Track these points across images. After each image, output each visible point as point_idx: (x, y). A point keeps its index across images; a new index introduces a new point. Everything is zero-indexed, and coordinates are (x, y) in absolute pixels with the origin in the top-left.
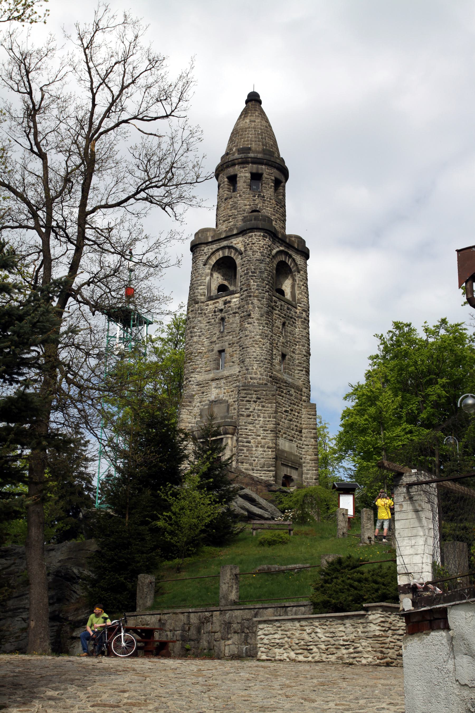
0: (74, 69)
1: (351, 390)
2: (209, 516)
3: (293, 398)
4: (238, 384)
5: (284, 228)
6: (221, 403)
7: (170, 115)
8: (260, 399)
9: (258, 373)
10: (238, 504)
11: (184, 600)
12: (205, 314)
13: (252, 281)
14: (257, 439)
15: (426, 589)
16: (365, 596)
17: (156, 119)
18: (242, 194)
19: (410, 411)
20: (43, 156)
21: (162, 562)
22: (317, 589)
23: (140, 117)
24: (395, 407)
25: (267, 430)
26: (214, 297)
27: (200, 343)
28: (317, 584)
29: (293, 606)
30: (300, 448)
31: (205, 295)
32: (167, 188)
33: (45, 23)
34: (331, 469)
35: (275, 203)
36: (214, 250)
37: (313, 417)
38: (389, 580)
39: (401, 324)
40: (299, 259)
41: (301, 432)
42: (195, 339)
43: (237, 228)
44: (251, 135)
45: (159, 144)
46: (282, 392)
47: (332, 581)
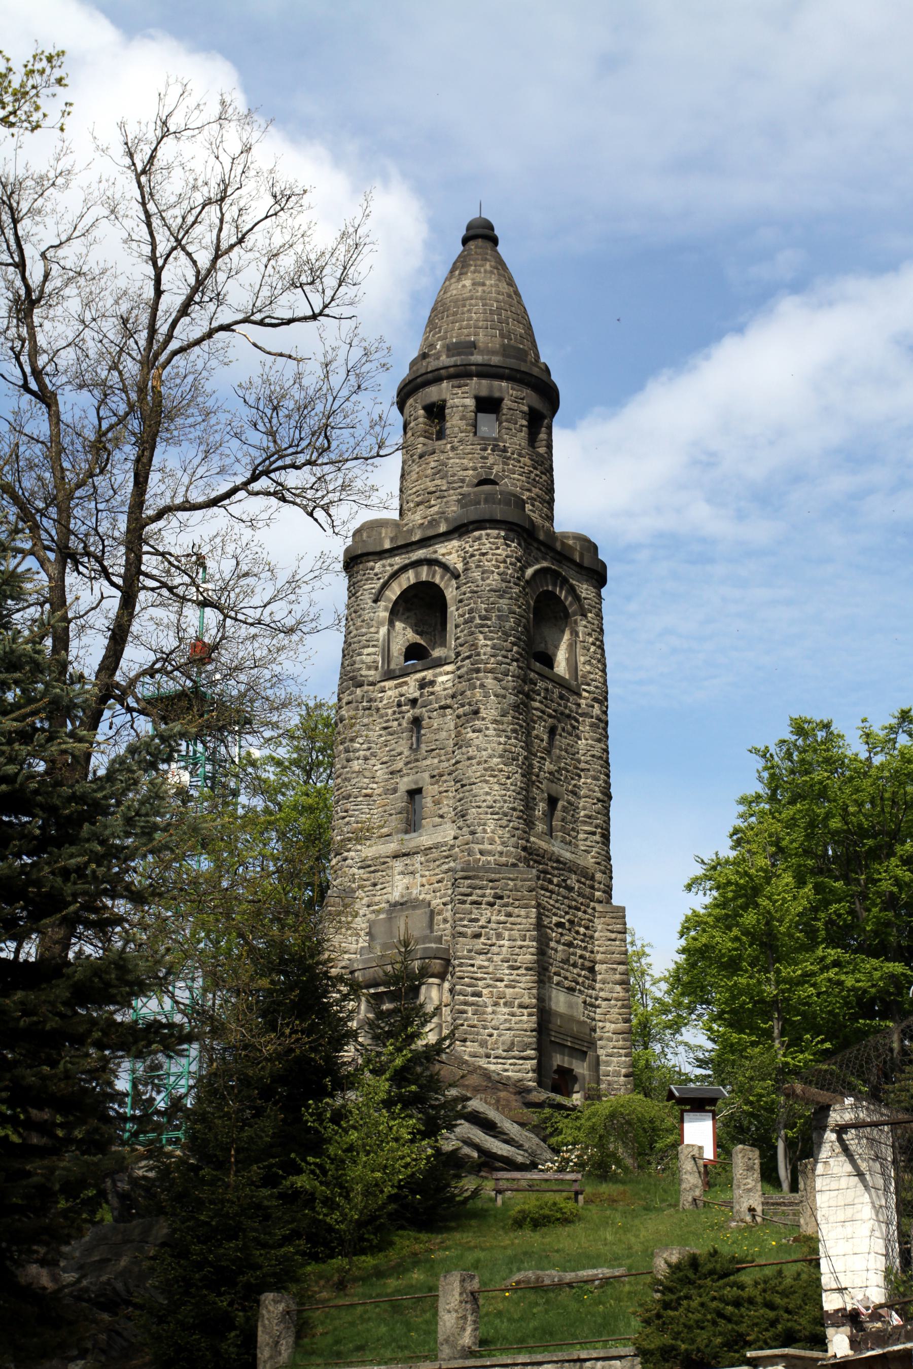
0: (112, 212)
1: (699, 870)
2: (406, 1166)
3: (574, 895)
4: (452, 864)
5: (550, 518)
6: (414, 908)
7: (321, 314)
8: (501, 898)
9: (495, 839)
10: (458, 1137)
11: (360, 1348)
12: (378, 710)
13: (481, 637)
14: (496, 987)
15: (876, 1316)
16: (748, 1335)
17: (290, 322)
18: (456, 444)
19: (834, 917)
20: (47, 398)
21: (303, 1265)
22: (647, 1322)
23: (258, 317)
24: (800, 909)
25: (519, 968)
26: (397, 673)
27: (367, 774)
28: (647, 1311)
29: (597, 1359)
30: (592, 1005)
31: (376, 668)
32: (318, 470)
33: (62, 129)
34: (657, 1048)
35: (529, 462)
36: (396, 567)
37: (619, 936)
38: (799, 1302)
39: (810, 722)
40: (585, 590)
41: (592, 970)
42: (356, 765)
43: (446, 520)
44: (476, 313)
45: (298, 377)
46: (551, 882)
47: (680, 1304)
